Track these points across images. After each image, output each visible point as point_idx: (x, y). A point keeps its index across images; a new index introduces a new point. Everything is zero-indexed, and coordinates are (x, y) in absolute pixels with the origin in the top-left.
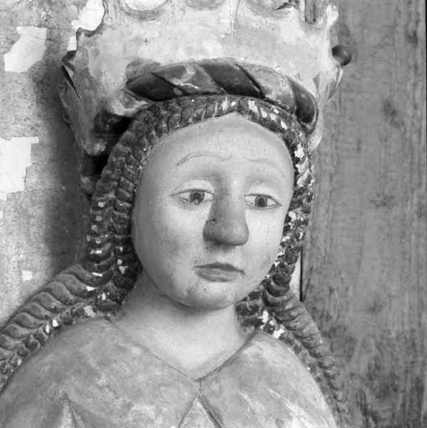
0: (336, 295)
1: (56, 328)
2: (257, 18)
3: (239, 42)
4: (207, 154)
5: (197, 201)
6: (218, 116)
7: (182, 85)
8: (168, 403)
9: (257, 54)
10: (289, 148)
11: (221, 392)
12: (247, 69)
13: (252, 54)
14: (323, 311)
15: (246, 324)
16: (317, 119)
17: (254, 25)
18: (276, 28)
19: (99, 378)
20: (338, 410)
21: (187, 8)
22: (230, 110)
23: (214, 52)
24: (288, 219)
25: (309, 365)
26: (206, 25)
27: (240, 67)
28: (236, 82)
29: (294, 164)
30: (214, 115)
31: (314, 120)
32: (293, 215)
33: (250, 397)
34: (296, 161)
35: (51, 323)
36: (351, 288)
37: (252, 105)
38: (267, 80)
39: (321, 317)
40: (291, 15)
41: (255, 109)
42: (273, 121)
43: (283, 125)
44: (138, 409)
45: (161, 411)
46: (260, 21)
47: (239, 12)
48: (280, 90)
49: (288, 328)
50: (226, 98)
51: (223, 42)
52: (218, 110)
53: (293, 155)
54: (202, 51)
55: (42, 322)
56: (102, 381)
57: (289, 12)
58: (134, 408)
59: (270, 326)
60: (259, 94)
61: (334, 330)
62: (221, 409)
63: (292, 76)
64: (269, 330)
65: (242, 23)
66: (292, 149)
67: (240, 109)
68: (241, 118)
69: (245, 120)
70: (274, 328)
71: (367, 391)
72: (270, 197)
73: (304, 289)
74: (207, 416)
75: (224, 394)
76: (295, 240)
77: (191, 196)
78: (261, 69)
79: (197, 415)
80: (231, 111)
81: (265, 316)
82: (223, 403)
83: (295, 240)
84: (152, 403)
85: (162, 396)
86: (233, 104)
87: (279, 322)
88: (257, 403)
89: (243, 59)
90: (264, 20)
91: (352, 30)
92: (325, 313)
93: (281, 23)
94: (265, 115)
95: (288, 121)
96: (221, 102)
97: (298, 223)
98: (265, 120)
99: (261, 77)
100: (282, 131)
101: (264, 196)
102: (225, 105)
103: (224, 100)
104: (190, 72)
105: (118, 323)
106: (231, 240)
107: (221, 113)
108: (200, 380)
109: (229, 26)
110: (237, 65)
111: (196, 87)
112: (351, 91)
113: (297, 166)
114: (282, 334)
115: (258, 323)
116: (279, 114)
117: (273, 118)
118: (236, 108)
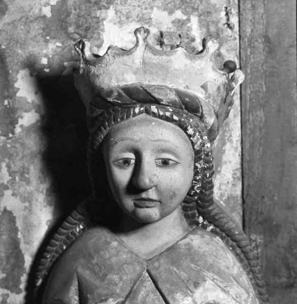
0: (266, 199)
1: (82, 229)
2: (156, 57)
3: (145, 72)
4: (127, 139)
5: (127, 165)
6: (133, 116)
7: (112, 101)
8: (127, 274)
9: (156, 78)
10: (183, 130)
11: (159, 267)
12: (147, 89)
13: (153, 79)
14: (258, 209)
15: (191, 224)
16: (202, 110)
17: (154, 61)
18: (170, 61)
19: (94, 259)
20: (252, 272)
21: (115, 56)
22: (140, 112)
23: (131, 80)
24: (196, 168)
25: (231, 246)
26: (126, 65)
27: (143, 88)
28: (141, 96)
29: (189, 138)
30: (131, 116)
31: (201, 111)
32: (197, 165)
33: (178, 269)
34: (190, 136)
35: (79, 227)
36: (276, 195)
37: (154, 108)
38: (159, 94)
39: (257, 213)
40: (178, 53)
41: (155, 111)
42: (167, 116)
43: (175, 118)
44: (110, 277)
45: (122, 278)
46: (158, 58)
47: (145, 55)
48: (169, 99)
49: (215, 225)
50: (138, 106)
51: (135, 73)
52: (133, 113)
53: (187, 133)
54: (124, 80)
55: (74, 226)
56: (95, 261)
57: (177, 50)
58: (109, 277)
59: (204, 225)
60: (157, 102)
61: (265, 221)
62: (158, 277)
63: (182, 88)
64: (204, 227)
65: (147, 61)
66: (185, 130)
67: (147, 112)
68: (148, 116)
69: (150, 117)
70: (207, 225)
71: (289, 256)
72: (170, 159)
73: (245, 197)
74: (151, 281)
75: (161, 268)
76: (205, 178)
77: (123, 162)
78: (155, 88)
79: (146, 280)
80: (142, 113)
81: (201, 219)
82: (160, 273)
83: (205, 178)
84: (118, 274)
85: (124, 270)
86: (142, 109)
87: (210, 223)
88: (182, 273)
89: (147, 83)
90: (160, 58)
91: (272, 39)
92: (259, 210)
93: (173, 58)
94: (161, 113)
95: (178, 114)
96: (134, 109)
97: (204, 169)
98: (162, 116)
99: (155, 93)
100: (175, 121)
101: (167, 159)
102: (137, 110)
103: (136, 107)
104: (116, 94)
105: (180, 207)
106: (147, 187)
107: (135, 115)
108: (147, 261)
109: (139, 64)
110: (141, 87)
111: (119, 102)
112: (273, 76)
113: (191, 138)
114: (212, 229)
115: (197, 223)
116: (173, 111)
117: (168, 114)
118: (144, 111)
